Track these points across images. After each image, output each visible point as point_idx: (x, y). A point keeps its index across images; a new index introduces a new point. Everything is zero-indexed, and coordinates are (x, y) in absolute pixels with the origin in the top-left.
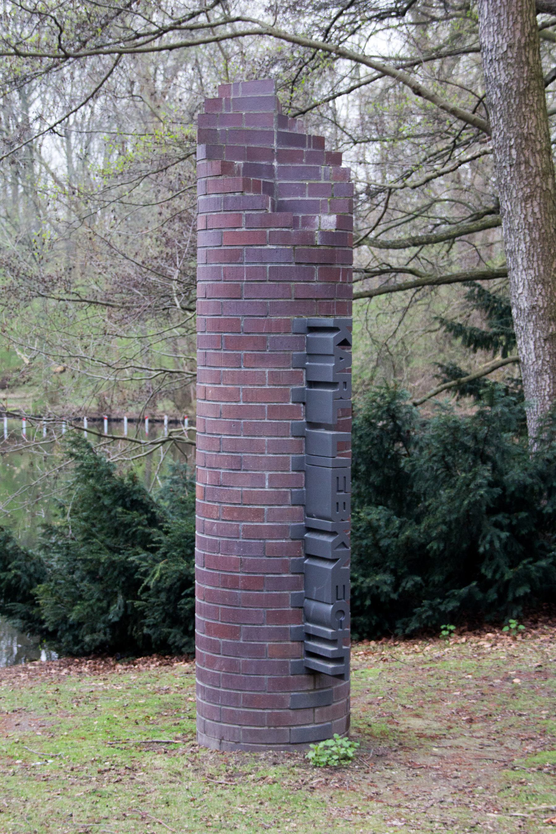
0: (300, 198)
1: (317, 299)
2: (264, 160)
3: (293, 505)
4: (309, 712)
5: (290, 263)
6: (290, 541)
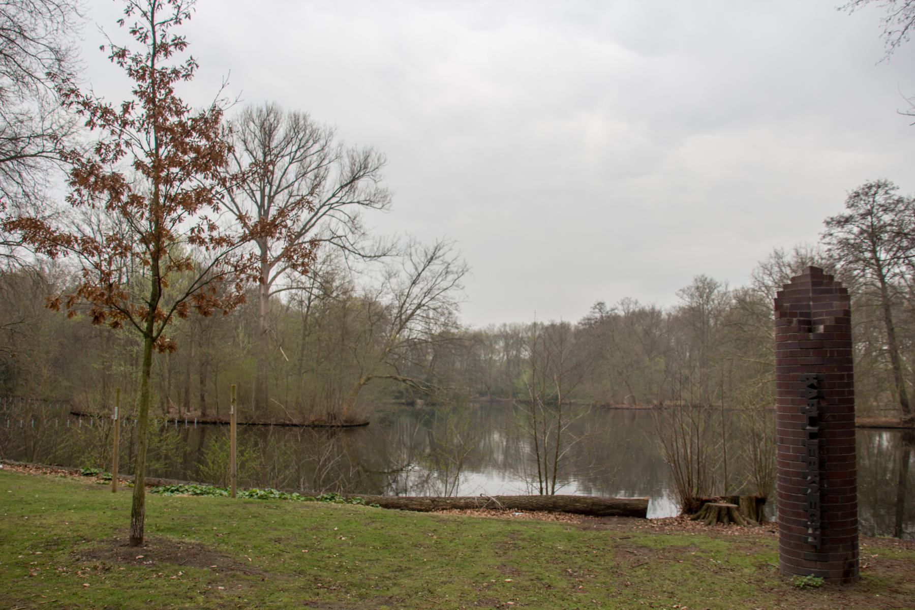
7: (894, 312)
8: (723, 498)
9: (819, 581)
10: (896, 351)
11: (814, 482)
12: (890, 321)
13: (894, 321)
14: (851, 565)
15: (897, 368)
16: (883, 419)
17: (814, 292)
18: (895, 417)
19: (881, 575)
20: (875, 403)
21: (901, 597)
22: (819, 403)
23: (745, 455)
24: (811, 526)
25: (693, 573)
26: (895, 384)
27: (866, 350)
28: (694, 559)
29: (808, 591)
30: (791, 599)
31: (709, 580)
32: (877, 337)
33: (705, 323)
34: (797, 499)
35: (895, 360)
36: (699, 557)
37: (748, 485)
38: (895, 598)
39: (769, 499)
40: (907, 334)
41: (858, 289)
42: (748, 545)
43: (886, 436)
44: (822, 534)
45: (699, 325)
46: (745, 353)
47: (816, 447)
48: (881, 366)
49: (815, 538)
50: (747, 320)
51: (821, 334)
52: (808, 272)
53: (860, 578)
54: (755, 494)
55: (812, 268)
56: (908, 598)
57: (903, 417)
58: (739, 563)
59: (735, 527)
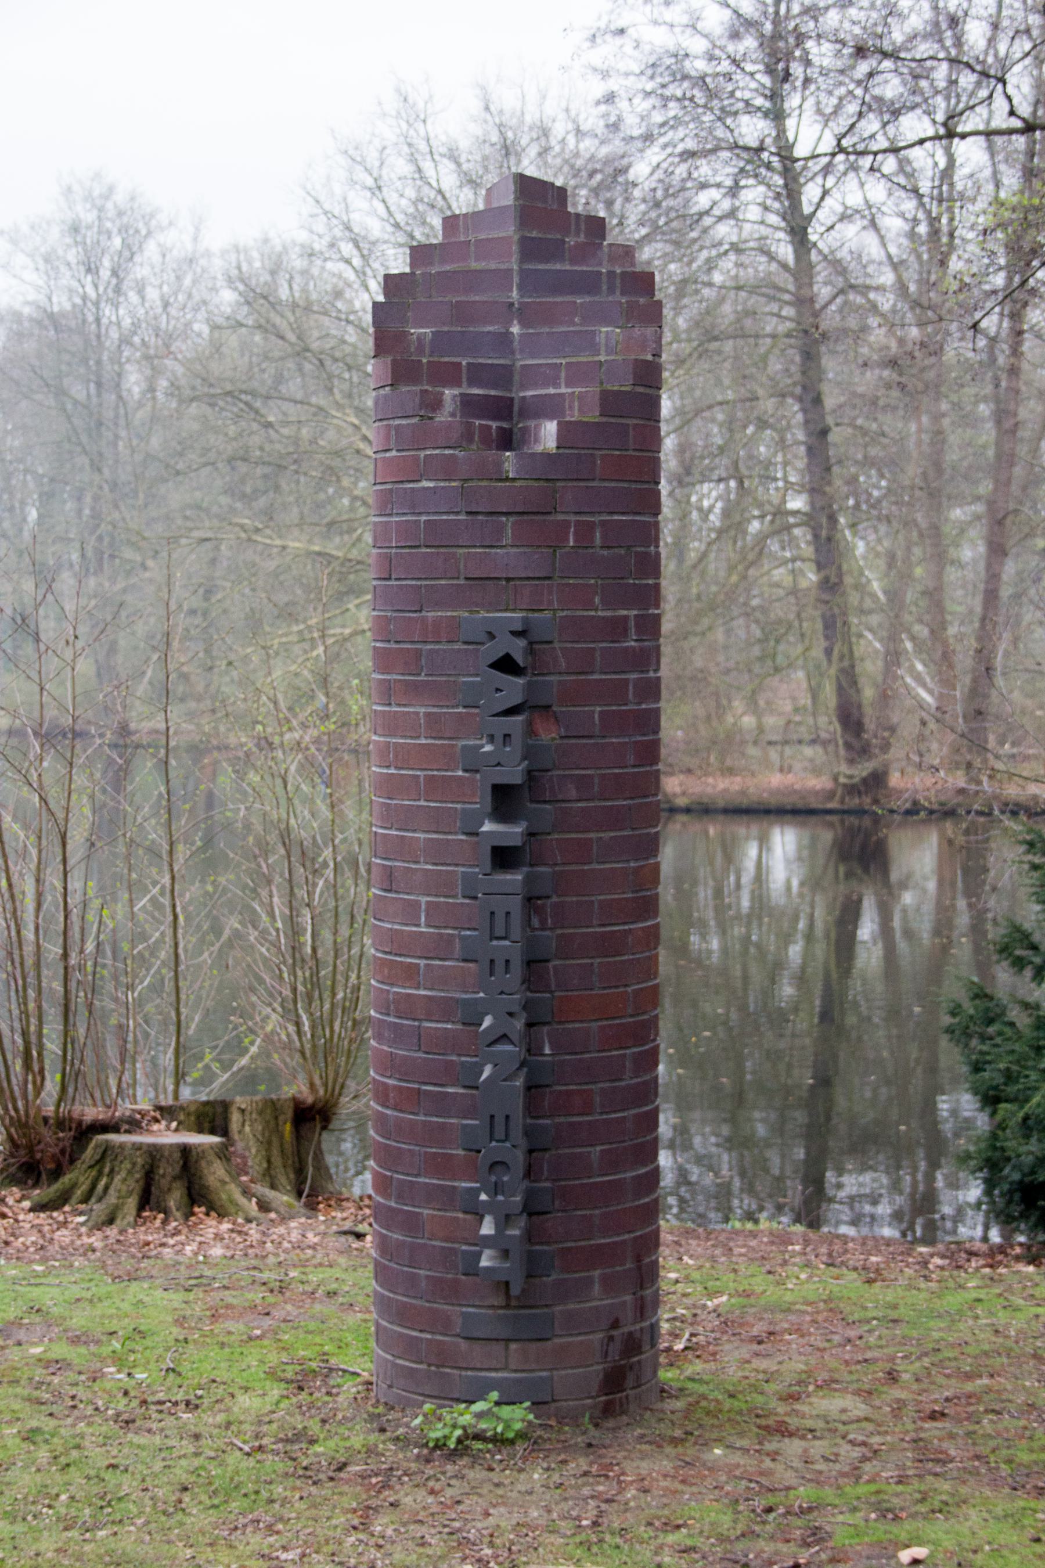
0: (552, 391)
1: (508, 580)
2: (491, 323)
3: (465, 960)
4: (498, 1348)
5: (458, 513)
6: (460, 1027)
7: (831, 366)
8: (166, 1112)
9: (517, 1416)
10: (832, 519)
11: (504, 1038)
12: (818, 401)
13: (830, 402)
14: (633, 1345)
15: (831, 585)
16: (776, 780)
17: (529, 282)
18: (816, 771)
19: (733, 1373)
20: (738, 715)
21: (793, 1447)
22: (530, 731)
23: (253, 936)
24: (490, 1208)
25: (30, 1437)
26: (820, 645)
27: (726, 513)
28: (39, 1374)
29: (476, 1459)
30: (411, 1498)
31: (99, 1458)
32: (768, 464)
33: (104, 382)
34: (441, 1104)
35: (828, 551)
36: (59, 1365)
37: (265, 1050)
38: (774, 1456)
39: (347, 1106)
40: (874, 451)
41: (710, 266)
42: (256, 1296)
43: (784, 843)
44: (530, 1236)
45: (78, 391)
46: (269, 514)
47: (515, 904)
48: (779, 574)
49: (505, 1254)
50: (279, 379)
51: (546, 456)
52: (508, 199)
53: (663, 1392)
54: (297, 1088)
55: (526, 185)
56: (819, 1448)
57: (844, 768)
58: (222, 1375)
59: (211, 1226)
